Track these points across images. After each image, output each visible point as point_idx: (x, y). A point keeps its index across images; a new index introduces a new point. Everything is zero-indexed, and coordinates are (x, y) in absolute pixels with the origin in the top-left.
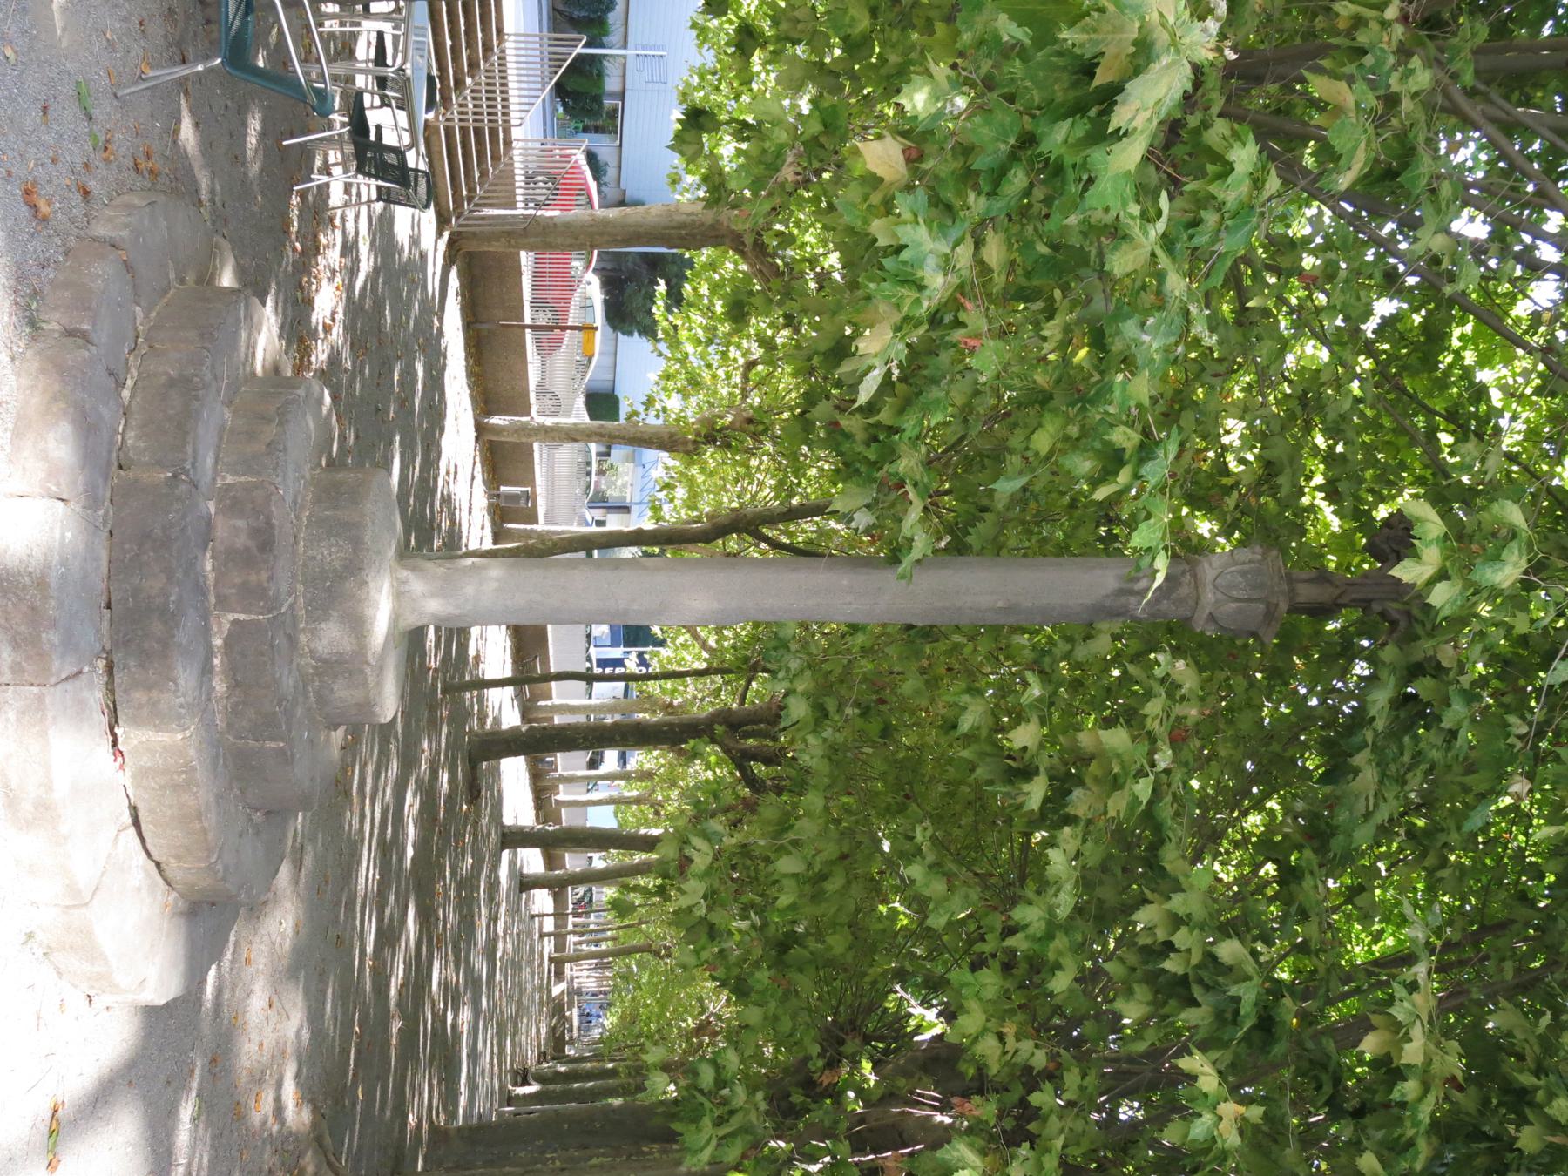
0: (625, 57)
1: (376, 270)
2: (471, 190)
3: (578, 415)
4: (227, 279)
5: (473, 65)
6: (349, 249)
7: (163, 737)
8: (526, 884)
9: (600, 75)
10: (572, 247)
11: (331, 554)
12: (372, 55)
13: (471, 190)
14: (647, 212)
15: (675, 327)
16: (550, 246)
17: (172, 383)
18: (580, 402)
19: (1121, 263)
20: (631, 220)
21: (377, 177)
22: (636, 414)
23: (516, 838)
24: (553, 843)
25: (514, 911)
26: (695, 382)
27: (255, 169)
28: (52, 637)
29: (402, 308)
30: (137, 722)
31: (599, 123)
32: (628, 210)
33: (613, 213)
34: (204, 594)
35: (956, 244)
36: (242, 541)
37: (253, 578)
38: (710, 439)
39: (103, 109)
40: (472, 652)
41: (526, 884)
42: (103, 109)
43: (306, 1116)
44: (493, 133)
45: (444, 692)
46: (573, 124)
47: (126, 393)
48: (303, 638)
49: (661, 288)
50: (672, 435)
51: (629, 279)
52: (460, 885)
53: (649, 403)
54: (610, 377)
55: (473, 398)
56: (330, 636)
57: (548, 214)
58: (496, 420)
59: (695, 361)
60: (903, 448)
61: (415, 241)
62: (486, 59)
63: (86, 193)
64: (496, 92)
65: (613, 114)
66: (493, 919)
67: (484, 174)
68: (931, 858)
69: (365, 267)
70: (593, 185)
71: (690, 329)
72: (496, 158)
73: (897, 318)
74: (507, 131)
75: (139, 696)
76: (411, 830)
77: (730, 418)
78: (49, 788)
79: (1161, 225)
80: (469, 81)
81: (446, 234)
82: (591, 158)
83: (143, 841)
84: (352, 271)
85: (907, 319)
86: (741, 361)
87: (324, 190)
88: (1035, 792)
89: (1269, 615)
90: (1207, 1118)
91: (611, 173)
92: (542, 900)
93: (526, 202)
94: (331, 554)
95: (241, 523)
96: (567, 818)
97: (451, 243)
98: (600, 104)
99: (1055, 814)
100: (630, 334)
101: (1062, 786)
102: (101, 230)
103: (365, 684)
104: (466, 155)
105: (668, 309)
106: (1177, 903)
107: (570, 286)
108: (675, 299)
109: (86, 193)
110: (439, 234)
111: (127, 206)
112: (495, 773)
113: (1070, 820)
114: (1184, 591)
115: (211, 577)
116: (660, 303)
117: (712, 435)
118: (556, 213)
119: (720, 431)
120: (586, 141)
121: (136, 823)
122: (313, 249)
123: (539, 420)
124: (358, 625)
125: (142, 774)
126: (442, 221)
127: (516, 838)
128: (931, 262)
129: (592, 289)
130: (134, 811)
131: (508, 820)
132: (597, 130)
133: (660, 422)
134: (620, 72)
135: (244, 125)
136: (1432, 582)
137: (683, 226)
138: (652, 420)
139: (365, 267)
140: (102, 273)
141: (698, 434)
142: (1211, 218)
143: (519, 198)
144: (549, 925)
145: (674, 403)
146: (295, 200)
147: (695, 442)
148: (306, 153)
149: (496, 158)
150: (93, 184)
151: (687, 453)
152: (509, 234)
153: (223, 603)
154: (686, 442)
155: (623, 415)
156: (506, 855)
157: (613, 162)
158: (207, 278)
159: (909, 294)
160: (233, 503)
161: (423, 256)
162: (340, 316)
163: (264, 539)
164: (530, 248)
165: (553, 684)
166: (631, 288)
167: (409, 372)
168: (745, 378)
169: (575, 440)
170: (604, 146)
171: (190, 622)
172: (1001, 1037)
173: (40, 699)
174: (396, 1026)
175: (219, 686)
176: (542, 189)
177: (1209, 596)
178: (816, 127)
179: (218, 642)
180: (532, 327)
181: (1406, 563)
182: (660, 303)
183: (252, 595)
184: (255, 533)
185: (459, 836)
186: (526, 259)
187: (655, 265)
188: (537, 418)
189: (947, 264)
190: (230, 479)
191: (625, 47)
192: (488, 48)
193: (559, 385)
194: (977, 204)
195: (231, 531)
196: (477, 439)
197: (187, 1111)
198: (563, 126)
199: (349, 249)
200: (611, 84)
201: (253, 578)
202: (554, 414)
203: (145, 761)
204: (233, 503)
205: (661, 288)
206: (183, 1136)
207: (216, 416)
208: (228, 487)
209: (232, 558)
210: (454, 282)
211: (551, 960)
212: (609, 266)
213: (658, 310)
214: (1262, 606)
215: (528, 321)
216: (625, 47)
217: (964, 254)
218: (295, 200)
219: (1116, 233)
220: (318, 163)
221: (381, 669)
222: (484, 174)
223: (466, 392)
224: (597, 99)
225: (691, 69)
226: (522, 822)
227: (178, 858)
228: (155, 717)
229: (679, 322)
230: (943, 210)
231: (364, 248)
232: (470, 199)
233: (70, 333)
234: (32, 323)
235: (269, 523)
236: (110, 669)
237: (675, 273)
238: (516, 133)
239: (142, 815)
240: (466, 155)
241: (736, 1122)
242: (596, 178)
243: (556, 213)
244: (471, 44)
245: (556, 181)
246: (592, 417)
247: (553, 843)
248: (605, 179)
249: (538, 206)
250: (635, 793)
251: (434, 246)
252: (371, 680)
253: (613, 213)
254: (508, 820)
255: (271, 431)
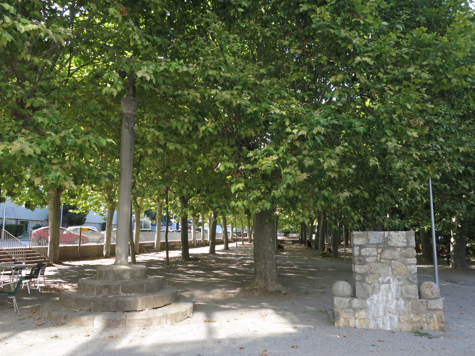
0: (6, 219)
1: (61, 278)
2: (42, 258)
3: (104, 233)
4: (58, 299)
5: (9, 257)
6: (55, 283)
7: (140, 303)
8: (227, 248)
9: (11, 225)
10: (59, 233)
11: (111, 276)
12: (9, 276)
13: (42, 258)
14: (50, 214)
15: (82, 208)
16: (58, 239)
17: (76, 303)
18: (102, 232)
19: (58, 142)
20: (52, 218)
21: (38, 275)
22: (104, 218)
23: (213, 251)
24: (214, 242)
25: (232, 251)
26: (97, 203)
27: (35, 298)
28: (118, 318)
29: (72, 273)
30: (137, 307)
31: (25, 226)
32: (49, 219)
33: (50, 223)
34: (115, 297)
35: (53, 170)
36: (107, 291)
37: (113, 288)
38: (111, 200)
39: (22, 317)
40: (163, 260)
41: (227, 248)
42: (22, 317)
43: (238, 289)
44: (27, 252)
45: (169, 265)
46: (25, 233)
47: (77, 310)
48: (127, 281)
49: (71, 211)
50: (110, 209)
51: (70, 219)
52: (217, 262)
53: (102, 215)
54: (98, 225)
55: (98, 259)
56: (127, 276)
57: (49, 239)
58: (104, 253)
59: (92, 203)
60: (92, 174)
61: (55, 271)
62: (7, 254)
63: (39, 319)
64: (16, 251)
65: (22, 222)
66: (231, 256)
67: (38, 255)
68: (178, 167)
69: (60, 280)
70: (42, 228)
71: (83, 204)
72: (34, 252)
73: (64, 180)
74: (27, 249)
75: (132, 306)
76: (196, 272)
77: (106, 195)
78: (144, 319)
79: (53, 134)
80: (13, 258)
81: (54, 264)
82: (35, 228)
83: (159, 308)
84: (60, 283)
85: (64, 179)
86: (92, 191)
87: (41, 287)
88: (160, 150)
89: (134, 100)
90: (209, 129)
91: (39, 223)
92: (230, 245)
93: (46, 245)
94: (111, 276)
95: (103, 291)
96: (208, 239)
97: (56, 263)
98: (19, 225)
99: (164, 147)
100: (85, 219)
101: (160, 146)
102: (46, 316)
103: (136, 270)
104: (33, 259)
105: (77, 209)
106: (179, 128)
107: (70, 234)
108: (74, 208)
109: (39, 319)
110: (54, 266)
111: (42, 312)
112: (192, 254)
113: (165, 144)
114: (129, 116)
115: (113, 296)
116: (75, 211)
117: (110, 199)
118: (49, 237)
119: (109, 197)
120: (30, 228)
121: (156, 308)
122: (54, 289)
123: (105, 242)
124: (125, 271)
125: (146, 307)
126: (50, 265)
127: (213, 251)
128: (55, 174)
129: (70, 229)
130: (154, 308)
131: (208, 252)
132: (27, 227)
133: (107, 212)
134: (10, 220)
135: (25, 300)
136: (117, 90)
137: (54, 206)
138: (106, 214)
139: (60, 280)
140: (54, 314)
141: (110, 203)
142: (51, 124)
143: (45, 246)
144: (241, 243)
145: (102, 208)
146: (43, 292)
147: (112, 204)
148: (31, 290)
149: (34, 252)
150: (37, 318)
151: (115, 205)
152: (55, 249)
153: (117, 294)
154: (112, 206)
155: (105, 221)
156: (216, 253)
157: (36, 223)
158: (57, 301)
159: (60, 178)
160: (99, 292)
161: (59, 269)
162: (71, 284)
163: (106, 287)
164: (58, 244)
165: (169, 241)
166: (73, 219)
167: (87, 272)
168: (96, 191)
169: (110, 234)
170: (31, 225)
171: (120, 299)
172: (209, 156)
173: (129, 320)
174: (237, 274)
175: (133, 294)
176: (43, 241)
177: (130, 112)
178: (32, 188)
179: (125, 295)
180: (80, 244)
181: (113, 94)
182: (75, 211)
183: (117, 288)
184: (105, 288)
185: (206, 262)
186: (61, 245)
187: (65, 212)
188: (104, 243)
189: (57, 171)
190: (95, 293)
191: (3, 219)
192: (4, 253)
193: (97, 237)
194: (46, 166)
195: (104, 292)
196: (109, 258)
197: (223, 306)
198: (25, 236)
199: (55, 283)
200: (13, 222)
201: (113, 288)
202: (104, 238)
203: (144, 306)
204: (99, 292)
205: (71, 211)
206: (227, 307)
207: (84, 296)
208: (97, 293)
209: (109, 293)
210: (67, 263)
211: (250, 242)
212: (66, 224)
213: (77, 212)
214: (132, 102)
215: (78, 245)
216: (3, 219)
217: (55, 167)
218: (43, 292)
219: (53, 143)
220: (34, 288)
221: (134, 267)
222: (38, 255)
223: (96, 260)
224: (18, 226)
225: (12, 202)
226: (209, 249)
227: (164, 302)
228: (136, 304)
229: (81, 207)
230: (48, 172)
231: (55, 281)
232: (45, 258)
233: (65, 318)
234: (63, 324)
235: (103, 286)
236: (127, 311)
237: (67, 207)
238: (28, 247)
239: (154, 307)
240: (33, 259)
241: (226, 205)
242: (40, 227)
243: (49, 237)
244: (4, 257)
245: (41, 238)
246: (105, 230)
247: (214, 242)
248: (41, 225)
249: (47, 242)
250: (208, 221)
251: (57, 267)
252: (136, 269)
253: (50, 223)
254: (208, 252)
255: (87, 287)
